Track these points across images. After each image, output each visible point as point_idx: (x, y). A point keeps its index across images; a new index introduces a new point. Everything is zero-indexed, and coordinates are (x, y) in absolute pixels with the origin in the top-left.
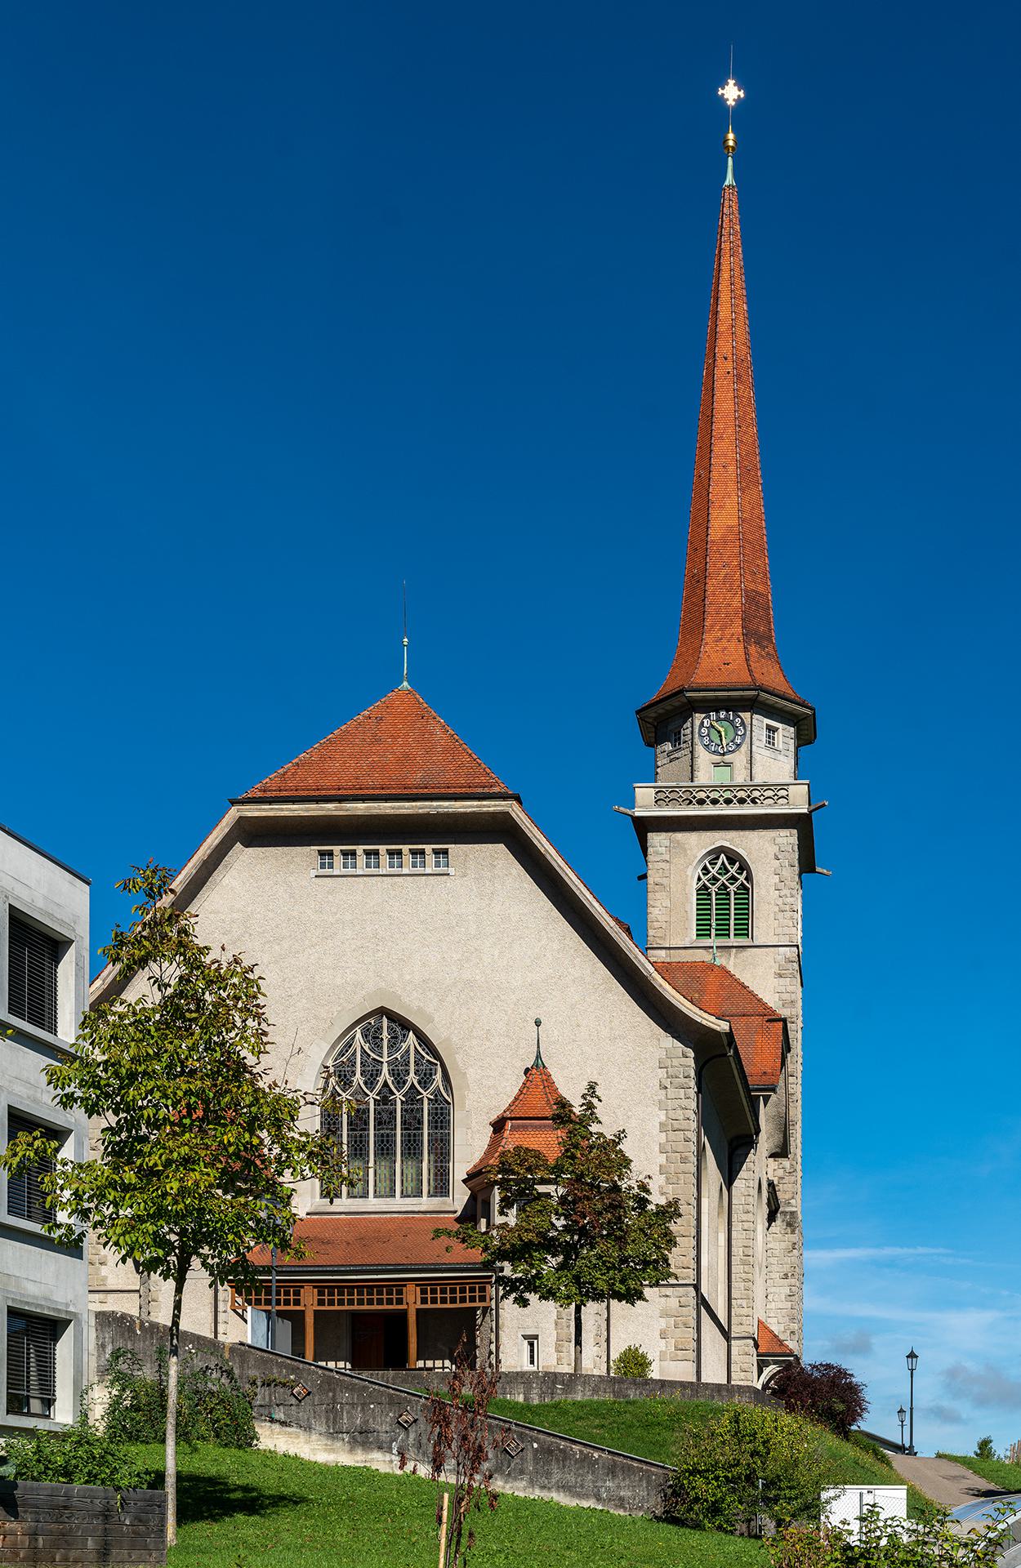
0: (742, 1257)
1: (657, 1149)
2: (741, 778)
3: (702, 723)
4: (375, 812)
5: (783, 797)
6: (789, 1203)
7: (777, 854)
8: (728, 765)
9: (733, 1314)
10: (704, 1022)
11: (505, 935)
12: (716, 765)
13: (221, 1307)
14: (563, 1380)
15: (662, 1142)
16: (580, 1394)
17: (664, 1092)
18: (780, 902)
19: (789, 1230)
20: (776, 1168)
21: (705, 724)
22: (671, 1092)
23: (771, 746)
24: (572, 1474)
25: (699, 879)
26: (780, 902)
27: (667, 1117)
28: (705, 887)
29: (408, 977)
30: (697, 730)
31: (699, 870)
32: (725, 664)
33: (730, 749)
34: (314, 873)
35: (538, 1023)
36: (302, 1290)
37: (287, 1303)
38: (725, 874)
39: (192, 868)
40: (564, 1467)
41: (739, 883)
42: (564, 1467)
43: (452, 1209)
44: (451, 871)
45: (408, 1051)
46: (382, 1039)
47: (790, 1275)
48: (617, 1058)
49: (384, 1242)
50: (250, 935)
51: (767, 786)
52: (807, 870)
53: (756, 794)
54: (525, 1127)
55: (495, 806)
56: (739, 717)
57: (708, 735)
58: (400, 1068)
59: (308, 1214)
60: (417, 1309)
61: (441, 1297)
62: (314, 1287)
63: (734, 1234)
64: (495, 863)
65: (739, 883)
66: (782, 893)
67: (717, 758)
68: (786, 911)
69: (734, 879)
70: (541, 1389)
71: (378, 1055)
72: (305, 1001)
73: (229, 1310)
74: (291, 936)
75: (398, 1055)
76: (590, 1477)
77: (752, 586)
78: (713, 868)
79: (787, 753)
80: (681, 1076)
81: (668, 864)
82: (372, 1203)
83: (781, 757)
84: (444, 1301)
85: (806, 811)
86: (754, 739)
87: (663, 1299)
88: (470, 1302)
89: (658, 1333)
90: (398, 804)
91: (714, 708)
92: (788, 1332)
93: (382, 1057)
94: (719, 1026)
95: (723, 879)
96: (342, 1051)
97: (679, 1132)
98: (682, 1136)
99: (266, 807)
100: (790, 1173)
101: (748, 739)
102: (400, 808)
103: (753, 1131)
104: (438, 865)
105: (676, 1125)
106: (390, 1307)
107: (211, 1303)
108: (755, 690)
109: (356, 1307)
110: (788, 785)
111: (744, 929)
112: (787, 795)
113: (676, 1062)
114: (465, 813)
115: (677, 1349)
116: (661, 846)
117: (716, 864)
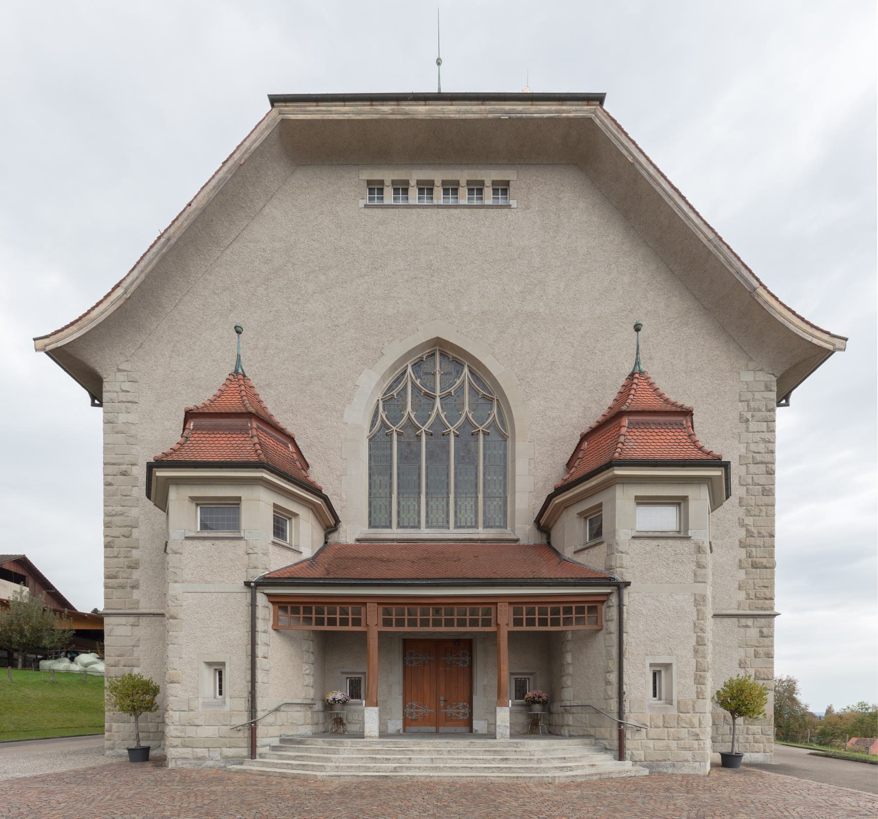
10: (815, 341)
13: (260, 625)
17: (744, 425)
22: (753, 426)
29: (465, 309)
34: (362, 203)
35: (637, 328)
36: (363, 609)
37: (332, 622)
43: (513, 537)
49: (455, 561)
54: (646, 424)
55: (576, 111)
59: (358, 540)
60: (509, 632)
61: (408, 619)
62: (379, 604)
64: (561, 196)
72: (353, 331)
73: (271, 630)
74: (337, 266)
80: (764, 410)
82: (425, 532)
84: (437, 623)
87: (742, 630)
88: (539, 626)
89: (738, 662)
93: (434, 393)
96: (391, 386)
98: (764, 469)
99: (312, 108)
102: (466, 112)
109: (407, 629)
113: (758, 396)
114: (542, 119)
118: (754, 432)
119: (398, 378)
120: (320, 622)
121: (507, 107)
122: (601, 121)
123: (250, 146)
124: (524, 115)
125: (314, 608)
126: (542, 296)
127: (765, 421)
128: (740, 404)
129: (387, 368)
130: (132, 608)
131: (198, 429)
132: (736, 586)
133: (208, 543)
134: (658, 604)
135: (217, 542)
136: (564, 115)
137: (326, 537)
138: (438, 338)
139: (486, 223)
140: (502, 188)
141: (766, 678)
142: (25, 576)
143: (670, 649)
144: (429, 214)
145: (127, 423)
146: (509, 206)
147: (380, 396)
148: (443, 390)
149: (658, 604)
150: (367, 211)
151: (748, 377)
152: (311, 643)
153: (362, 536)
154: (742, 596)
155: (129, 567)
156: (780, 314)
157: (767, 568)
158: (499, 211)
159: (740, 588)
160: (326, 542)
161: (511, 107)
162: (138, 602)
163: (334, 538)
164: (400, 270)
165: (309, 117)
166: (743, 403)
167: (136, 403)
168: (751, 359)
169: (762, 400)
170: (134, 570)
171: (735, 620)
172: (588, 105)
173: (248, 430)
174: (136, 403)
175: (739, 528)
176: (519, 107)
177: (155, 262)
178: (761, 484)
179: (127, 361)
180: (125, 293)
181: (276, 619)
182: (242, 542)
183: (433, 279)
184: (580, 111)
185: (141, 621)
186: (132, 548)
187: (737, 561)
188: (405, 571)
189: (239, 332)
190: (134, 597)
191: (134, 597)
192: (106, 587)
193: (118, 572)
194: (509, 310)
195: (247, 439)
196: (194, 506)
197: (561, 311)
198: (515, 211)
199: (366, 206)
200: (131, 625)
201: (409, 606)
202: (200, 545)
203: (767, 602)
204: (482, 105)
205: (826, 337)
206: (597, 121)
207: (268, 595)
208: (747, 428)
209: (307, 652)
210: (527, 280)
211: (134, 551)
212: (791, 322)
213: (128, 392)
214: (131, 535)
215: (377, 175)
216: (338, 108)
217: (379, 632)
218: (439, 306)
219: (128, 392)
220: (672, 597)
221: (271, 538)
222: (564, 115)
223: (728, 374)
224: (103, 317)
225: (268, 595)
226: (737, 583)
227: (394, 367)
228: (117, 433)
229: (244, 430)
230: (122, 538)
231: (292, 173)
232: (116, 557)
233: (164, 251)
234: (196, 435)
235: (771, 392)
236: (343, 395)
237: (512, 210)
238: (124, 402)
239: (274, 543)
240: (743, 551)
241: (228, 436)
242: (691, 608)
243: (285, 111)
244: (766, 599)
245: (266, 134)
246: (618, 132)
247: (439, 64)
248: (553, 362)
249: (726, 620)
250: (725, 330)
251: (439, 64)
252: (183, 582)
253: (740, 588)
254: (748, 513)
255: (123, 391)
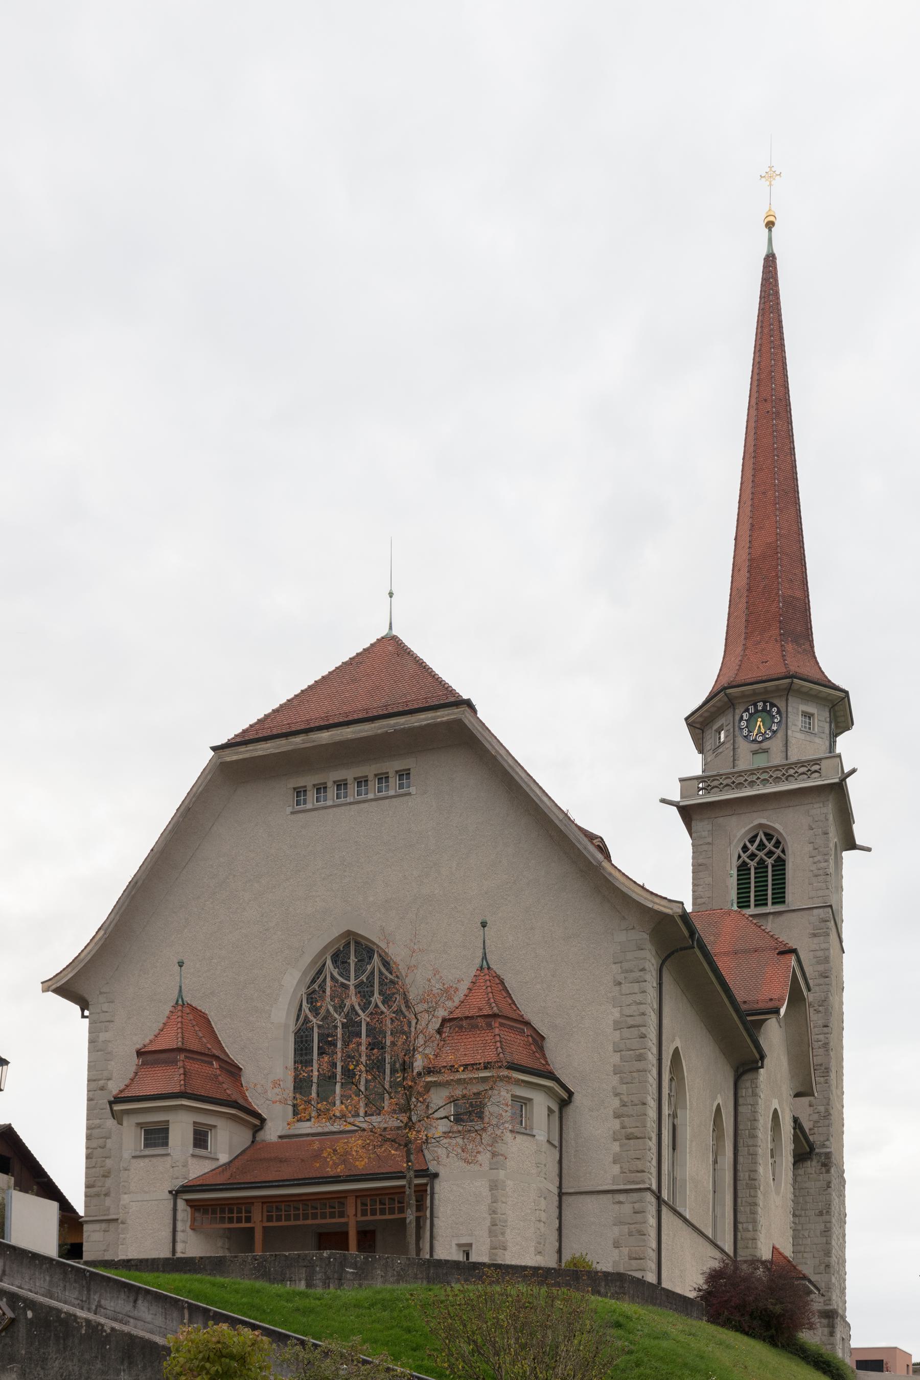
0: (748, 1182)
1: (611, 1048)
2: (777, 759)
3: (742, 717)
4: (338, 738)
5: (816, 771)
6: (824, 1145)
7: (811, 824)
8: (766, 751)
9: (739, 1237)
10: (656, 907)
11: (462, 846)
12: (755, 753)
14: (356, 1262)
15: (616, 1040)
16: (380, 1280)
17: (617, 988)
18: (814, 868)
19: (824, 1170)
20: (812, 1112)
21: (745, 718)
22: (625, 988)
23: (807, 730)
24: (75, 1360)
25: (739, 857)
26: (814, 868)
27: (622, 1015)
28: (744, 864)
29: (371, 899)
30: (737, 724)
31: (740, 849)
32: (763, 662)
33: (767, 736)
34: (289, 810)
38: (763, 849)
39: (180, 817)
40: (65, 1348)
41: (775, 856)
42: (65, 1348)
44: (412, 790)
45: (372, 973)
46: (349, 964)
47: (824, 1212)
48: (570, 957)
50: (234, 876)
51: (802, 764)
52: (848, 847)
53: (791, 772)
55: (448, 715)
56: (776, 706)
57: (747, 727)
58: (366, 989)
59: (280, 1137)
63: (741, 1159)
65: (775, 856)
66: (816, 859)
67: (755, 747)
68: (820, 875)
69: (752, 856)
70: (325, 1273)
71: (346, 979)
72: (279, 933)
73: (188, 1229)
75: (364, 978)
76: (99, 1366)
77: (790, 592)
78: (752, 846)
79: (823, 736)
81: (711, 846)
83: (817, 740)
85: (837, 780)
86: (790, 724)
87: (617, 1207)
90: (359, 728)
91: (753, 702)
92: (824, 1265)
93: (349, 981)
94: (672, 909)
95: (761, 854)
96: (314, 978)
97: (633, 1029)
99: (242, 750)
100: (824, 1116)
101: (783, 726)
102: (361, 731)
103: (757, 1056)
104: (401, 786)
105: (631, 1021)
106: (334, 1221)
107: (170, 1223)
108: (789, 678)
110: (820, 759)
111: (780, 898)
112: (820, 769)
115: (631, 1258)
116: (704, 831)
117: (754, 841)
118: (627, 995)
119: (320, 970)
120: (231, 1220)
121: (392, 721)
122: (469, 721)
123: (197, 791)
124: (406, 726)
125: (227, 1209)
126: (436, 878)
127: (637, 982)
128: (614, 966)
129: (307, 965)
130: (105, 1215)
131: (144, 1065)
132: (611, 1159)
133: (147, 1160)
134: (462, 1191)
135: (152, 1159)
136: (439, 720)
137: (254, 1137)
138: (348, 930)
139: (390, 812)
140: (404, 775)
141: (638, 1257)
142: (9, 1159)
143: (471, 1230)
144: (343, 811)
145: (104, 1042)
146: (409, 794)
147: (303, 990)
148: (357, 977)
149: (462, 1191)
150: (293, 816)
151: (621, 937)
152: (226, 1240)
153: (283, 1133)
154: (616, 1169)
155: (104, 1176)
156: (623, 884)
157: (638, 1138)
158: (401, 799)
159: (615, 1162)
160: (253, 1142)
161: (395, 721)
162: (108, 1209)
163: (261, 1136)
164: (318, 869)
165: (241, 757)
166: (616, 965)
167: (112, 1021)
168: (624, 918)
169: (635, 959)
170: (107, 1179)
171: (610, 1196)
172: (457, 708)
173: (177, 1062)
174: (112, 1021)
175: (613, 1098)
176: (402, 720)
177: (126, 903)
178: (633, 1048)
179: (107, 983)
180: (105, 933)
181: (193, 1220)
182: (169, 1157)
183: (345, 874)
184: (451, 714)
185: (110, 1226)
186: (106, 1158)
187: (611, 1132)
188: (287, 1172)
189: (181, 966)
190: (107, 1204)
191: (107, 1204)
192: (86, 1196)
193: (94, 1181)
194: (408, 896)
195: (176, 1070)
196: (139, 1129)
197: (453, 891)
198: (414, 797)
199: (292, 813)
200: (104, 1231)
201: (277, 1204)
202: (142, 1163)
203: (639, 1174)
204: (372, 723)
205: (664, 902)
206: (466, 722)
207: (187, 1200)
208: (620, 990)
209: (222, 1248)
210: (425, 864)
211: (107, 1161)
212: (633, 891)
213: (107, 1012)
214: (105, 1145)
215: (300, 782)
216: (262, 746)
217: (264, 1228)
218: (349, 899)
219: (107, 1012)
220: (473, 1184)
221: (191, 1149)
222: (439, 720)
223: (603, 936)
224: (89, 957)
225: (187, 1200)
226: (612, 1156)
227: (314, 962)
228: (98, 1051)
229: (174, 1062)
230: (99, 1149)
231: (235, 791)
232: (94, 1167)
233: (133, 893)
234: (143, 1070)
235: (642, 951)
236: (270, 996)
237: (412, 796)
238: (103, 1022)
239: (193, 1156)
240: (617, 1121)
241: (164, 1068)
242: (486, 1192)
243: (223, 755)
244: (638, 1172)
245: (209, 777)
246: (483, 729)
247: (391, 597)
248: (446, 942)
249: (601, 1196)
250: (600, 891)
251: (391, 597)
252: (129, 1194)
253: (615, 1162)
254: (622, 1082)
255: (104, 1012)
